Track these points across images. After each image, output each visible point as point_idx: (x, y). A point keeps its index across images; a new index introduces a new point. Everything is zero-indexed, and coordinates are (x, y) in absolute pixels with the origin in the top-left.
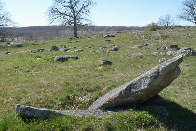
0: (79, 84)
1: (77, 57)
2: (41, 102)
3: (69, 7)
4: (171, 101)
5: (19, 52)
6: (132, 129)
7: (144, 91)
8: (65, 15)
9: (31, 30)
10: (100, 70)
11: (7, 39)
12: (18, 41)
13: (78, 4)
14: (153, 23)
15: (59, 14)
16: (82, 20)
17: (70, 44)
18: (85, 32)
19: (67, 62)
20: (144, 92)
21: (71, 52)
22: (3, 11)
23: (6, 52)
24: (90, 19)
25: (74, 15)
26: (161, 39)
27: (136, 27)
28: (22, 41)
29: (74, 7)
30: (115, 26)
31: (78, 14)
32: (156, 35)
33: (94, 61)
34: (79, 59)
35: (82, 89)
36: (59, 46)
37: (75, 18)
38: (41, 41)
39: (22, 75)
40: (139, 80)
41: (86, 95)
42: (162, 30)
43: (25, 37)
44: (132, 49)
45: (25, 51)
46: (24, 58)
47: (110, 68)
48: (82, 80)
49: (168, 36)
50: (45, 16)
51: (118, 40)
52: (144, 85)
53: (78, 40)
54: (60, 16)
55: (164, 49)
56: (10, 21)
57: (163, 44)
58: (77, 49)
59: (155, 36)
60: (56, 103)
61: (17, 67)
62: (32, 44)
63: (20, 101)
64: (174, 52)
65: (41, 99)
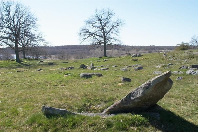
0: (96, 96)
1: (101, 74)
2: (62, 107)
3: (99, 27)
4: (168, 110)
5: (50, 70)
6: (126, 126)
7: (140, 98)
8: (95, 35)
9: (63, 49)
10: (119, 85)
11: (40, 57)
12: (50, 59)
13: (107, 25)
14: (183, 43)
15: (90, 35)
16: (112, 40)
17: (98, 63)
18: (116, 51)
19: (91, 78)
20: (140, 100)
21: (98, 70)
22: (38, 31)
23: (39, 69)
24: (119, 39)
25: (104, 35)
26: (188, 59)
27: (168, 47)
28: (54, 59)
29: (104, 27)
30: (146, 46)
31: (107, 34)
32: (183, 54)
33: (115, 78)
34: (103, 76)
35: (98, 100)
36: (88, 64)
37: (105, 38)
38: (72, 60)
39: (51, 88)
40: (136, 90)
41: (100, 104)
42: (191, 50)
43: (57, 56)
44: (156, 68)
45: (57, 69)
46: (54, 74)
47: (128, 85)
48: (100, 93)
49: (195, 56)
50: (76, 36)
51: (146, 59)
52: (139, 94)
53: (107, 60)
54: (90, 36)
55: (186, 68)
56: (44, 40)
57: (188, 64)
58: (104, 67)
59: (182, 55)
60: (74, 108)
61: (47, 81)
62: (63, 63)
63: (46, 105)
64: (193, 72)
65: (63, 105)
